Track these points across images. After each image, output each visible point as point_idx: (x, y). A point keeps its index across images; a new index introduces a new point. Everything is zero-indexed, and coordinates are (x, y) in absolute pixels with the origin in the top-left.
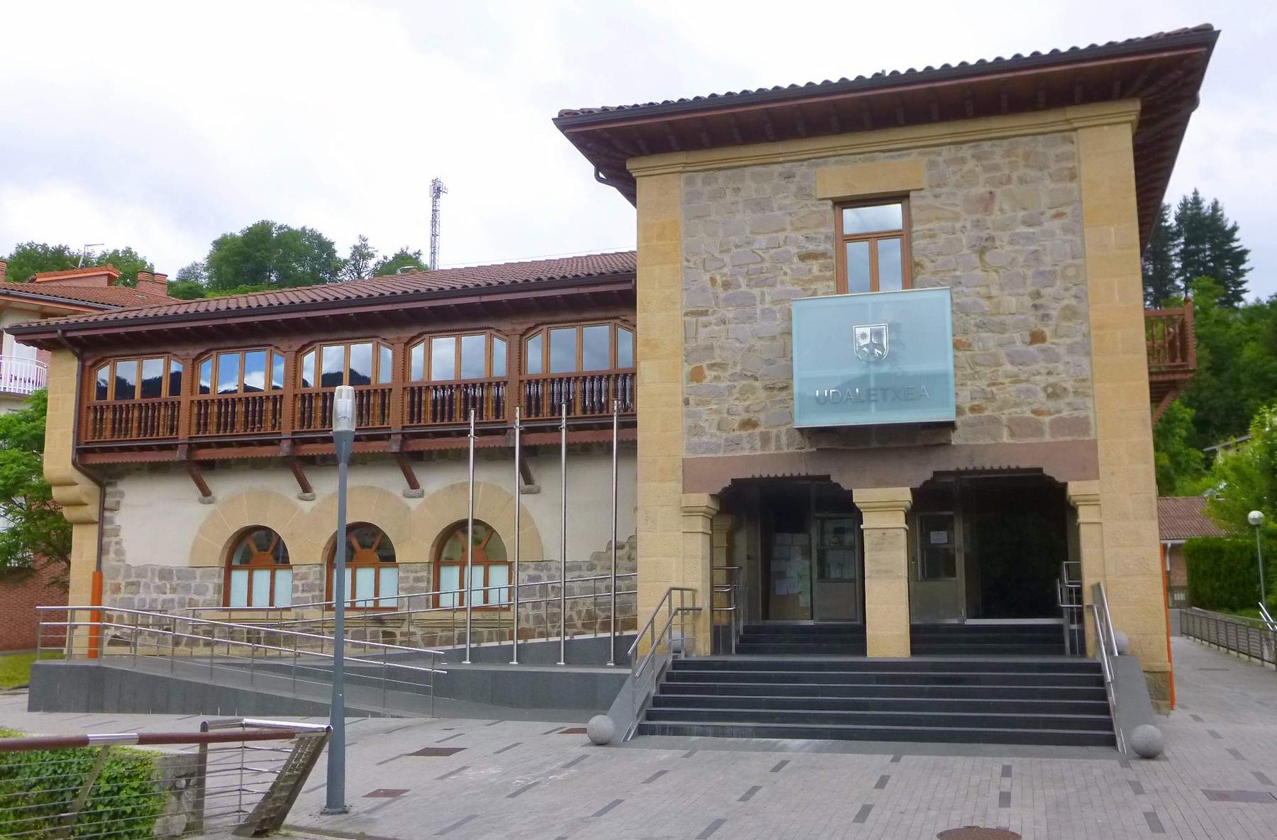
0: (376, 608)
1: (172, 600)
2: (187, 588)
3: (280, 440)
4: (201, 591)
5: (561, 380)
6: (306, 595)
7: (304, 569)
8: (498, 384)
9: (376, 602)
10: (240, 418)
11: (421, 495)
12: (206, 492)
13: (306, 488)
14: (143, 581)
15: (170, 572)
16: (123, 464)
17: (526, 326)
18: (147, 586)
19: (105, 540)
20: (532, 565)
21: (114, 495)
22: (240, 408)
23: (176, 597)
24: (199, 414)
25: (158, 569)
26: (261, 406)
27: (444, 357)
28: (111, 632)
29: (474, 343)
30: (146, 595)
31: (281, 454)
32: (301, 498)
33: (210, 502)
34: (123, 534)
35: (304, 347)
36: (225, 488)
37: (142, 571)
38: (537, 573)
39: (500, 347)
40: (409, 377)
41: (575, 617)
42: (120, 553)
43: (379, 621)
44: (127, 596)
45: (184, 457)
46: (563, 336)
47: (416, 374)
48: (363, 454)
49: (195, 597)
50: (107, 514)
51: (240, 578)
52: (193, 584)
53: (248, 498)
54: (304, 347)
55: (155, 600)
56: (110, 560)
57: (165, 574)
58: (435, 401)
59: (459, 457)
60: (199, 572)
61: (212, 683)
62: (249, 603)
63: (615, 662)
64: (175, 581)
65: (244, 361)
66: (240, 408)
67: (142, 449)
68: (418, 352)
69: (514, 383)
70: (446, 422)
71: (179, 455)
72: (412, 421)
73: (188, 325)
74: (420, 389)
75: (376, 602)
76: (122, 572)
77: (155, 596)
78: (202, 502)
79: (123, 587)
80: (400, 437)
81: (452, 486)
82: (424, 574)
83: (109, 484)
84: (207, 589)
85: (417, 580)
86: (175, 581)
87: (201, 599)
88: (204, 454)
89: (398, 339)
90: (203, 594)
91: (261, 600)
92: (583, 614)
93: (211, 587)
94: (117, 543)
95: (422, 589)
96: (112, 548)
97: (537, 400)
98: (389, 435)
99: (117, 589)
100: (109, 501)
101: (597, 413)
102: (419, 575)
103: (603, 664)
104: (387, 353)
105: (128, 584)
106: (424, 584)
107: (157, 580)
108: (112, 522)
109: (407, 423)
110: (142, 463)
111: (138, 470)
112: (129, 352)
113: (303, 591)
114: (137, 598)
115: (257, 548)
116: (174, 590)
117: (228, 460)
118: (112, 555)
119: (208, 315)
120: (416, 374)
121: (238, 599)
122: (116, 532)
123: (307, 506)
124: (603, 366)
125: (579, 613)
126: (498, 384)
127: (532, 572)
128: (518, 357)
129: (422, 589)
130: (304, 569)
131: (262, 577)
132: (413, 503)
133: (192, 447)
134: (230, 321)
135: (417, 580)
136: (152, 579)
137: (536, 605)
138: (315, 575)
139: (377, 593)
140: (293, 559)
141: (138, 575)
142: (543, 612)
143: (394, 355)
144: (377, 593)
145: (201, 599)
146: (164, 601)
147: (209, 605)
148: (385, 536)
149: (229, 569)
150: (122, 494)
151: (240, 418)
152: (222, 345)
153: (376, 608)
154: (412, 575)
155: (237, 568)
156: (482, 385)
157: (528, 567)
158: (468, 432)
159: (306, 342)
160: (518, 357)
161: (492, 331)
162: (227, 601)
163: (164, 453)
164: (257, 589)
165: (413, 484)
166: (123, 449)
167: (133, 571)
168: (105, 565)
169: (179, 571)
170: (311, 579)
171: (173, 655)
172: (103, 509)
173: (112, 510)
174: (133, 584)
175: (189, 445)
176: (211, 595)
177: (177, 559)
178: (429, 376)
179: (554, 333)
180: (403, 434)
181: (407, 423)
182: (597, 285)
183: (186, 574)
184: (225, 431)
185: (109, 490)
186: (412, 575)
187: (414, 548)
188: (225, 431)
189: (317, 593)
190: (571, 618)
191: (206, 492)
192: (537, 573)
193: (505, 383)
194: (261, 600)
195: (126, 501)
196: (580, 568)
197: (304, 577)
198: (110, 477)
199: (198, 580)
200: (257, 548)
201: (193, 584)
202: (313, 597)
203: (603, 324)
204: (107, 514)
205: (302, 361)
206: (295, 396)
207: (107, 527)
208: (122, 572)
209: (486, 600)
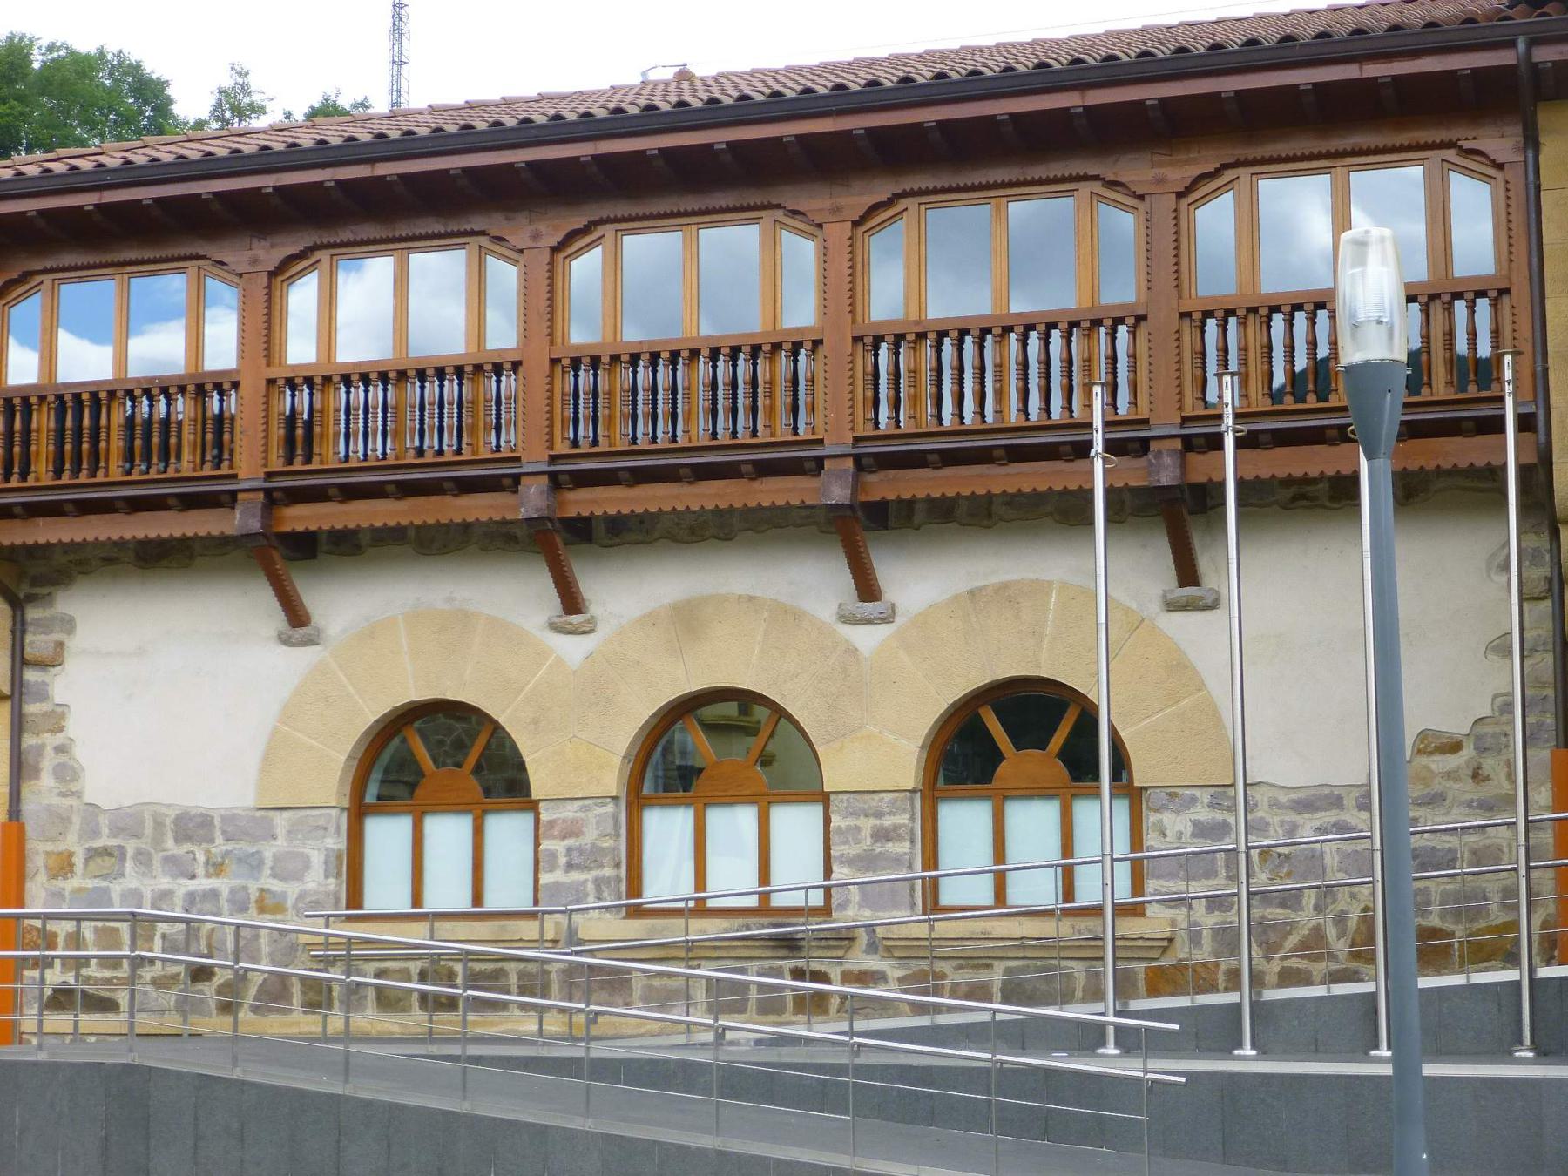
0: (764, 909)
1: (214, 894)
2: (253, 864)
3: (516, 478)
4: (289, 868)
5: (654, 358)
6: (576, 876)
7: (569, 812)
8: (498, 369)
9: (764, 897)
10: (43, 447)
11: (887, 619)
12: (296, 616)
13: (571, 602)
14: (131, 846)
15: (205, 821)
16: (72, 547)
17: (1196, 171)
18: (143, 858)
19: (29, 741)
20: (1205, 796)
21: (45, 626)
22: (44, 421)
23: (223, 885)
24: (60, 433)
25: (172, 813)
26: (96, 417)
27: (375, 308)
28: (56, 976)
29: (438, 272)
30: (136, 886)
31: (523, 513)
32: (556, 628)
33: (310, 642)
34: (73, 728)
35: (572, 236)
36: (346, 605)
37: (128, 822)
38: (1219, 816)
39: (504, 275)
40: (866, 305)
41: (1331, 932)
42: (68, 774)
43: (790, 944)
44: (90, 883)
45: (255, 525)
46: (649, 251)
47: (300, 351)
48: (718, 512)
49: (276, 886)
50: (31, 675)
51: (387, 837)
52: (269, 851)
53: (398, 633)
54: (572, 236)
55: (164, 896)
56: (42, 793)
57: (193, 827)
58: (291, 420)
59: (1071, 512)
60: (281, 821)
61: (465, 1107)
62: (477, 899)
63: (1535, 1046)
64: (220, 846)
65: (125, 294)
66: (44, 421)
67: (138, 505)
68: (302, 296)
69: (252, 386)
70: (83, 478)
71: (240, 520)
72: (58, 473)
73: (267, 182)
74: (95, 396)
75: (764, 897)
76: (76, 821)
77: (164, 883)
78: (285, 641)
79: (78, 860)
80: (849, 464)
81: (972, 593)
82: (903, 819)
83: (31, 599)
84: (307, 865)
85: (882, 835)
86: (220, 846)
87: (291, 890)
88: (300, 518)
89: (1160, 181)
90: (297, 876)
91: (447, 888)
92: (1353, 924)
93: (317, 859)
94: (60, 749)
95: (896, 861)
96: (48, 763)
97: (309, 425)
98: (820, 461)
99: (63, 866)
100: (36, 643)
101: (1312, 402)
102: (888, 822)
103: (1504, 1053)
104: (504, 275)
105: (92, 854)
106: (902, 848)
107: (170, 843)
108: (42, 695)
109: (277, 465)
110: (121, 544)
111: (109, 561)
112: (438, 227)
113: (570, 866)
114: (117, 888)
115: (437, 755)
116: (216, 868)
117: (355, 532)
118: (47, 780)
119: (76, 182)
120: (300, 351)
121: (386, 887)
122: (56, 720)
123: (572, 649)
124: (748, 322)
125: (1340, 922)
126: (498, 369)
127: (1203, 814)
128: (545, 303)
129: (896, 861)
130: (569, 812)
131: (448, 834)
132: (867, 639)
133: (274, 499)
134: (383, 169)
135: (882, 835)
136: (158, 841)
137: (1216, 903)
138: (600, 826)
139: (764, 875)
140: (540, 782)
141: (116, 831)
142: (1240, 917)
143: (825, 254)
144: (764, 875)
145: (291, 890)
146: (191, 899)
147: (316, 904)
148: (497, 727)
149: (358, 813)
150: (69, 625)
151: (43, 447)
152: (346, 235)
153: (764, 909)
154: (867, 825)
155: (651, 802)
156: (459, 371)
157: (1194, 800)
158: (1089, 445)
159: (578, 222)
160: (545, 303)
161: (483, 240)
162: (355, 895)
163: (195, 515)
164: (436, 862)
165: (867, 589)
166: (86, 508)
167: (104, 821)
168: (29, 806)
169: (230, 818)
170: (590, 836)
171: (40, 1033)
172: (20, 661)
173: (42, 665)
174: (106, 852)
175: (268, 492)
176: (319, 880)
177: (226, 787)
178: (921, 305)
179: (630, 242)
180: (857, 459)
181: (277, 465)
182: (372, 161)
183: (248, 827)
184: (76, 472)
185: (32, 613)
186: (867, 825)
187: (876, 747)
188: (76, 472)
189: (608, 872)
190: (1317, 935)
191: (296, 616)
192: (1219, 816)
193: (817, 343)
194: (447, 888)
195: (76, 643)
196: (1336, 802)
197: (571, 830)
198: (37, 581)
199: (281, 844)
200: (437, 755)
201: (269, 851)
202: (598, 883)
203: (749, 222)
204: (31, 675)
205: (1191, 222)
206: (554, 362)
207: (31, 708)
208: (76, 821)
209: (1069, 893)
